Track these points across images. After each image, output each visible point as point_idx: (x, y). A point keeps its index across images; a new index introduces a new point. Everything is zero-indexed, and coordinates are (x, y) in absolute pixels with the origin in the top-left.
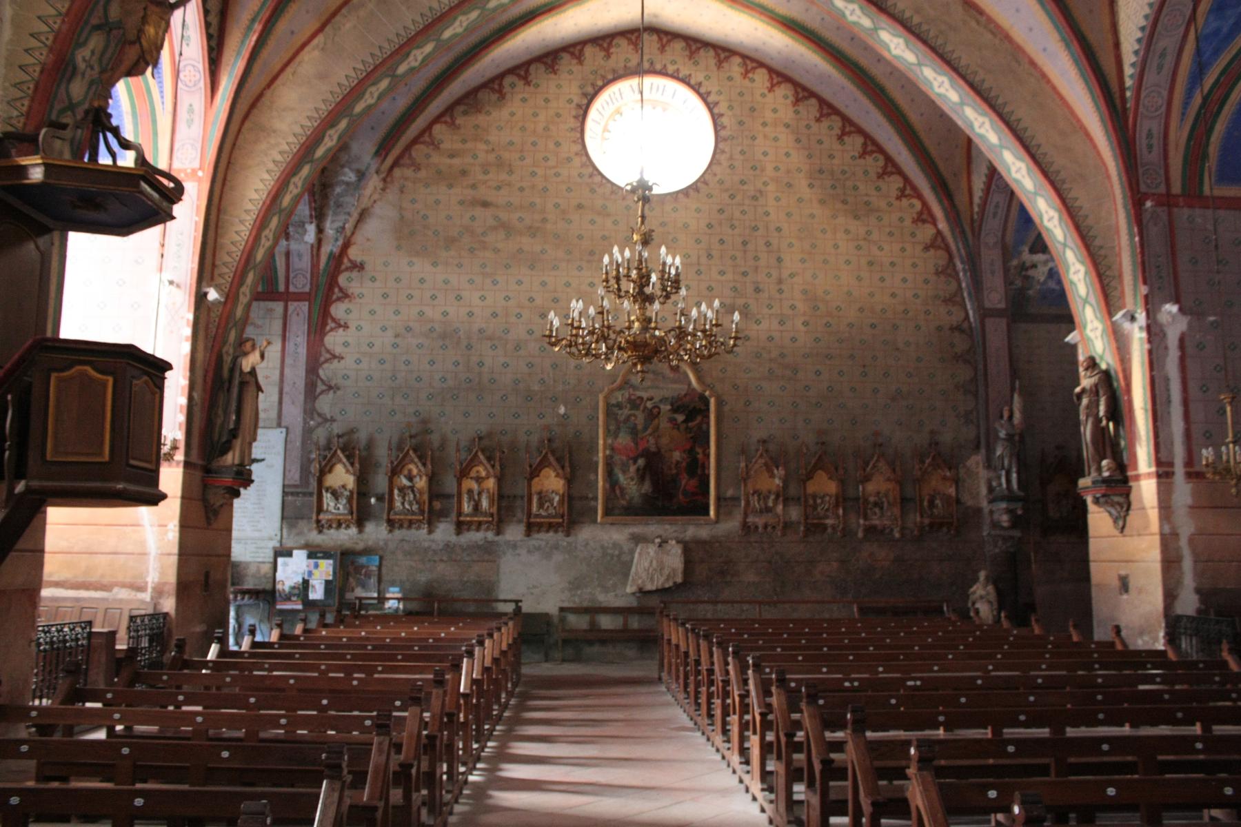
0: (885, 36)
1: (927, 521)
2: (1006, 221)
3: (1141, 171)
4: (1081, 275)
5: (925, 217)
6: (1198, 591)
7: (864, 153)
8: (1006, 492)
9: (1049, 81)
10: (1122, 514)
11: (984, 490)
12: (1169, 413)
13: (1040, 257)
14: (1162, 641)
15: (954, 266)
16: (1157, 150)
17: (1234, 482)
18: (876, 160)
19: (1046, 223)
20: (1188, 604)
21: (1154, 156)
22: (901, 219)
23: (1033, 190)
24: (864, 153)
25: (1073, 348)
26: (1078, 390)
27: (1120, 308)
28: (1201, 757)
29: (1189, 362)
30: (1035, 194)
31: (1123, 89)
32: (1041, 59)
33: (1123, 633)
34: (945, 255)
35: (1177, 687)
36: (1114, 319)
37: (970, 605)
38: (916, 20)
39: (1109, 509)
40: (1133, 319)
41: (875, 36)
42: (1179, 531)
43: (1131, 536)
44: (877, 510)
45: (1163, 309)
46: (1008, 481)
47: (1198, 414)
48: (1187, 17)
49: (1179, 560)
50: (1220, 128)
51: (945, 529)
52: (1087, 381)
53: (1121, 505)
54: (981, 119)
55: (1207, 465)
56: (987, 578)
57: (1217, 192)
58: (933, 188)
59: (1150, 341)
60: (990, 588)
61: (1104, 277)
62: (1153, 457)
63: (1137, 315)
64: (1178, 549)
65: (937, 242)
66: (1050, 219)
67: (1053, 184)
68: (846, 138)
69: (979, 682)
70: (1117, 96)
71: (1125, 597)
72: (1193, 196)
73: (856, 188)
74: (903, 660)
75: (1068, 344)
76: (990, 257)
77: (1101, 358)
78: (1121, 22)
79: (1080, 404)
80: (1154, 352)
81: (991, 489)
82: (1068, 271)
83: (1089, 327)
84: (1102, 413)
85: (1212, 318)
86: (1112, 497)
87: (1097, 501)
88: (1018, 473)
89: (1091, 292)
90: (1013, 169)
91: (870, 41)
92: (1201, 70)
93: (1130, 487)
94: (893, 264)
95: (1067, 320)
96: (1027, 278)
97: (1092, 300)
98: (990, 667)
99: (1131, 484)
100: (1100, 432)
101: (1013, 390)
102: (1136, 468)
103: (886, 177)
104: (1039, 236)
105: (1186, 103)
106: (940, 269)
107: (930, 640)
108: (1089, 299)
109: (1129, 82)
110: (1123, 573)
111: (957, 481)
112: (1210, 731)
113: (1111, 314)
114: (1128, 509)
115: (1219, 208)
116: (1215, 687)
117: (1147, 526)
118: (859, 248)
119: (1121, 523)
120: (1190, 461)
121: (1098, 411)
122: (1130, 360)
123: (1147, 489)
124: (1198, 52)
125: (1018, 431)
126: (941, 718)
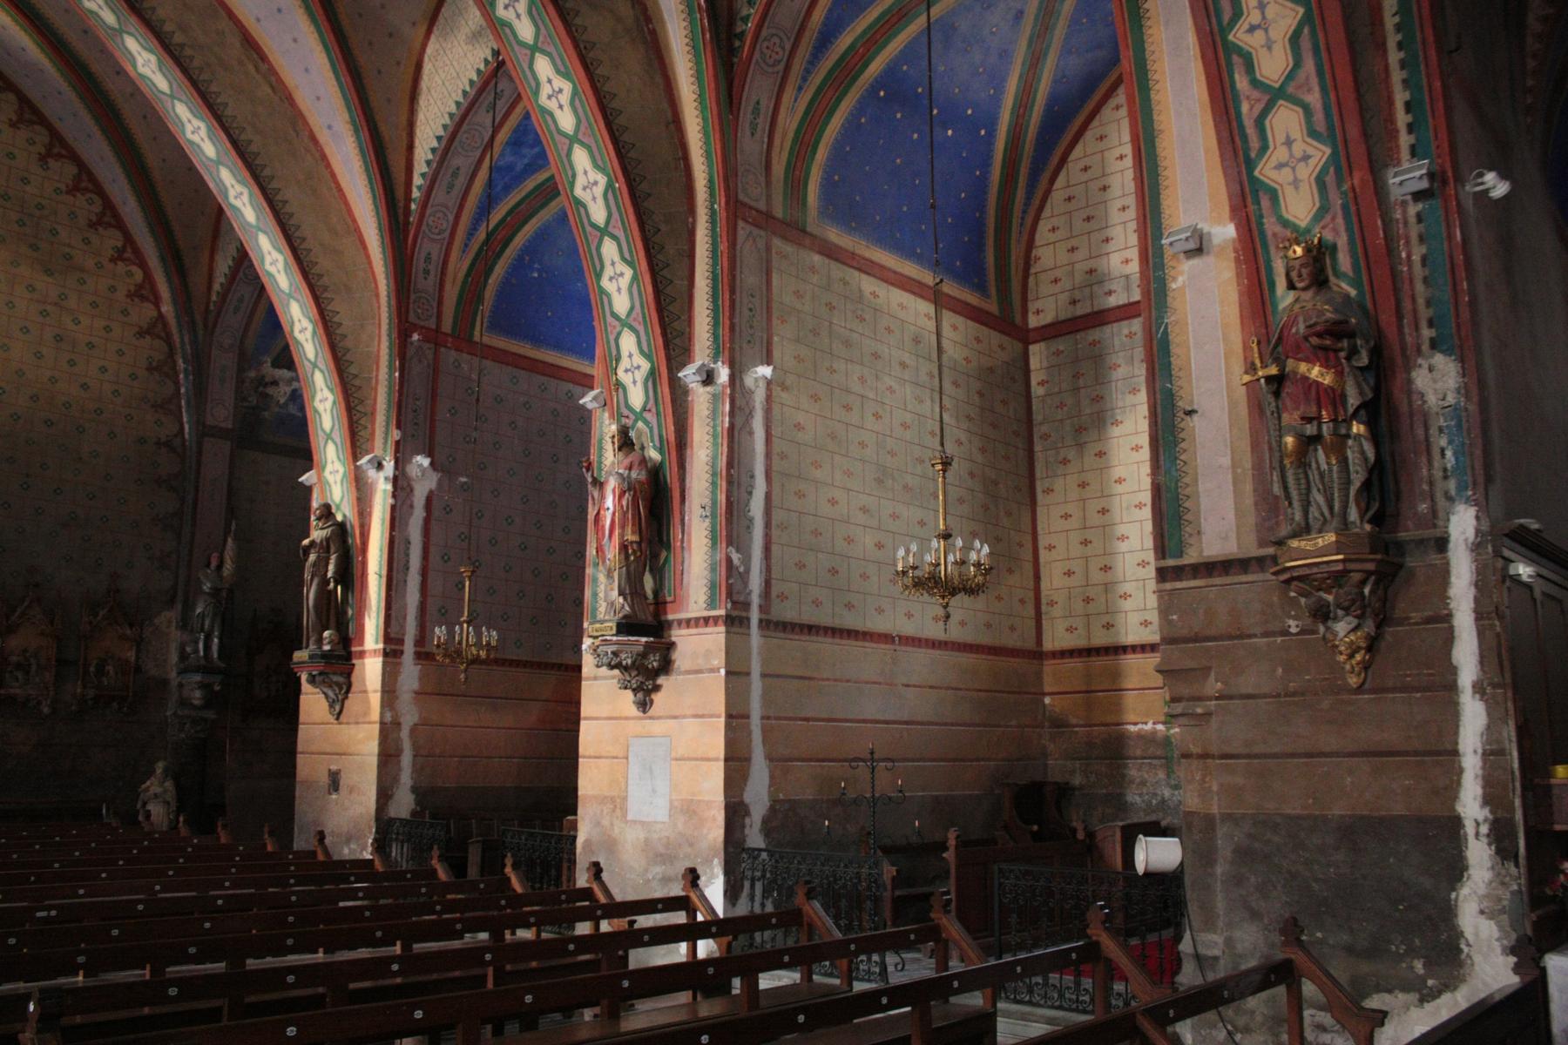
0: (132, 44)
1: (91, 693)
2: (248, 325)
3: (413, 297)
4: (329, 404)
5: (145, 292)
6: (414, 789)
7: (74, 189)
8: (203, 662)
9: (328, 165)
10: (340, 697)
11: (174, 658)
12: (405, 581)
13: (284, 373)
14: (370, 849)
15: (174, 362)
16: (432, 280)
17: (463, 667)
18: (90, 202)
19: (297, 334)
20: (403, 804)
21: (430, 284)
22: (113, 289)
23: (287, 291)
24: (74, 189)
25: (308, 490)
26: (306, 542)
27: (367, 453)
28: (399, 980)
29: (434, 524)
30: (290, 296)
31: (408, 199)
32: (324, 137)
33: (327, 841)
34: (166, 349)
35: (382, 902)
36: (358, 463)
37: (139, 805)
38: (178, 38)
39: (325, 690)
40: (380, 466)
41: (119, 40)
42: (402, 720)
43: (348, 723)
44: (20, 675)
45: (414, 461)
46: (207, 647)
47: (436, 585)
48: (485, 142)
49: (398, 754)
50: (499, 270)
51: (115, 705)
52: (317, 534)
53: (340, 686)
54: (239, 188)
55: (438, 646)
56: (166, 770)
57: (486, 340)
58: (163, 259)
59: (394, 496)
60: (169, 784)
61: (354, 412)
62: (381, 633)
63: (384, 463)
64: (399, 740)
65: (156, 328)
66: (303, 330)
67: (312, 288)
68: (52, 163)
69: (140, 907)
70: (401, 204)
71: (334, 796)
72: (463, 339)
73: (53, 232)
74: (34, 882)
75: (301, 484)
76: (223, 361)
77: (338, 507)
78: (418, 123)
79: (306, 560)
80: (398, 508)
81: (183, 656)
82: (313, 397)
83: (329, 468)
84: (330, 574)
85: (463, 479)
86: (331, 676)
87: (312, 680)
88: (221, 639)
89: (337, 427)
90: (268, 260)
91: (110, 44)
92: (490, 203)
93: (354, 665)
94: (91, 345)
95: (305, 456)
96: (266, 396)
97: (337, 436)
98: (158, 888)
99: (354, 661)
100: (325, 596)
101: (227, 533)
102: (362, 643)
103: (100, 229)
104: (286, 349)
105: (471, 233)
106: (154, 364)
107: (77, 854)
108: (333, 436)
109: (416, 194)
110: (334, 768)
111: (139, 643)
112: (411, 949)
113: (355, 457)
114: (348, 691)
115: (487, 358)
116: (422, 900)
117: (366, 713)
118: (44, 313)
119: (338, 708)
120: (421, 641)
121: (327, 571)
122: (370, 514)
123: (371, 670)
124: (490, 183)
125: (227, 586)
126: (81, 959)
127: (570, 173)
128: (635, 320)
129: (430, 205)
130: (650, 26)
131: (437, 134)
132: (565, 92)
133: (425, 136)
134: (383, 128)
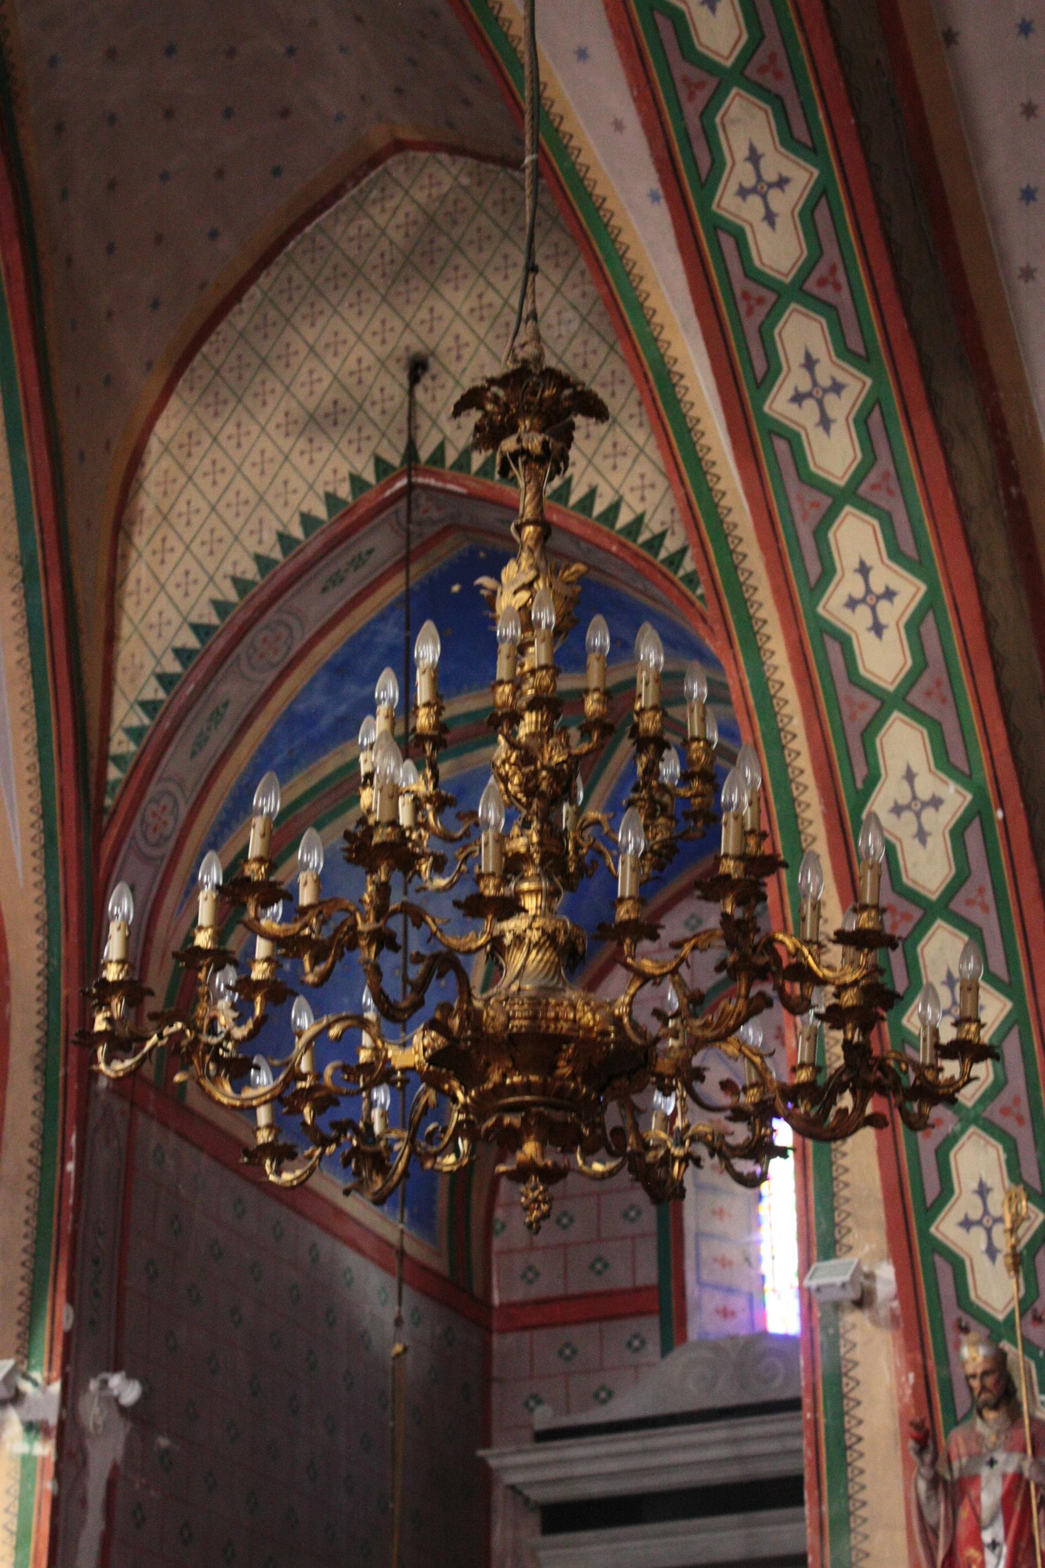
78: (130, 585)
109: (121, 744)
127: (861, 772)
128: (1005, 1111)
129: (156, 778)
130: (1013, 490)
131: (194, 618)
132: (900, 601)
133: (153, 618)
134: (79, 585)
